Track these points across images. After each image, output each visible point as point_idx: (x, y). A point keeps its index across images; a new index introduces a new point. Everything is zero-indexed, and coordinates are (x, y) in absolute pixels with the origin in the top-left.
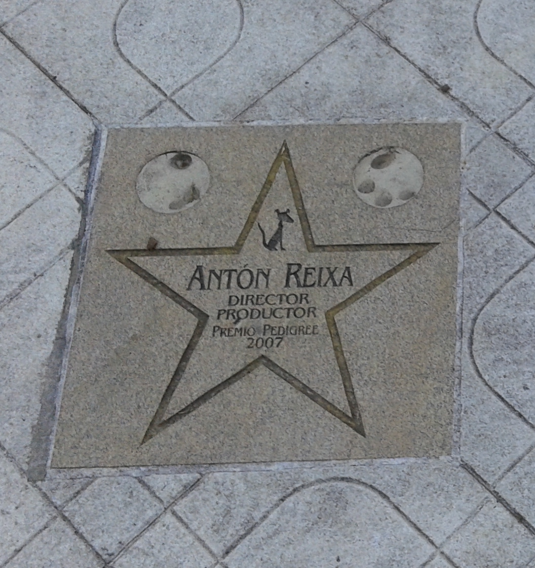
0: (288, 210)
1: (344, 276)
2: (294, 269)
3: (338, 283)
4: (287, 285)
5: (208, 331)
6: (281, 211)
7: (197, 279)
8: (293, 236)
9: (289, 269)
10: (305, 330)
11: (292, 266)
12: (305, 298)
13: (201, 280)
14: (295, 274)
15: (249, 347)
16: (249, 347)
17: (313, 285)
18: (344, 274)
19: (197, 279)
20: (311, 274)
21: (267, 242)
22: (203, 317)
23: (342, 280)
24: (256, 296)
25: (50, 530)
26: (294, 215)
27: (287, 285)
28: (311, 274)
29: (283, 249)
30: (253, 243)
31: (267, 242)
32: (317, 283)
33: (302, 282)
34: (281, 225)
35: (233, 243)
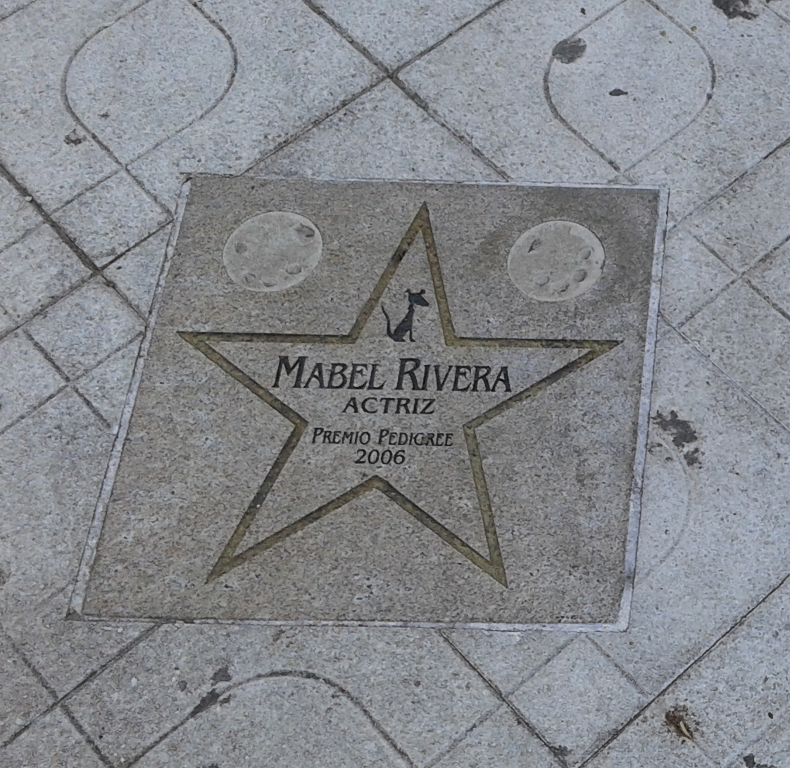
0: (423, 292)
1: (498, 379)
2: (409, 366)
3: (491, 386)
4: (399, 387)
5: (306, 438)
6: (414, 291)
7: (316, 377)
8: (426, 317)
9: (402, 367)
10: (332, 437)
11: (408, 363)
12: (405, 405)
13: (320, 378)
14: (484, 377)
15: (357, 462)
16: (357, 462)
17: (361, 387)
18: (313, 372)
19: (316, 377)
20: (464, 374)
21: (392, 332)
22: (300, 422)
23: (310, 380)
24: (413, 401)
25: (310, 667)
26: (429, 296)
27: (399, 387)
28: (464, 374)
29: (412, 340)
30: (377, 323)
31: (393, 328)
32: (472, 386)
33: (420, 386)
34: (411, 309)
35: (346, 329)
